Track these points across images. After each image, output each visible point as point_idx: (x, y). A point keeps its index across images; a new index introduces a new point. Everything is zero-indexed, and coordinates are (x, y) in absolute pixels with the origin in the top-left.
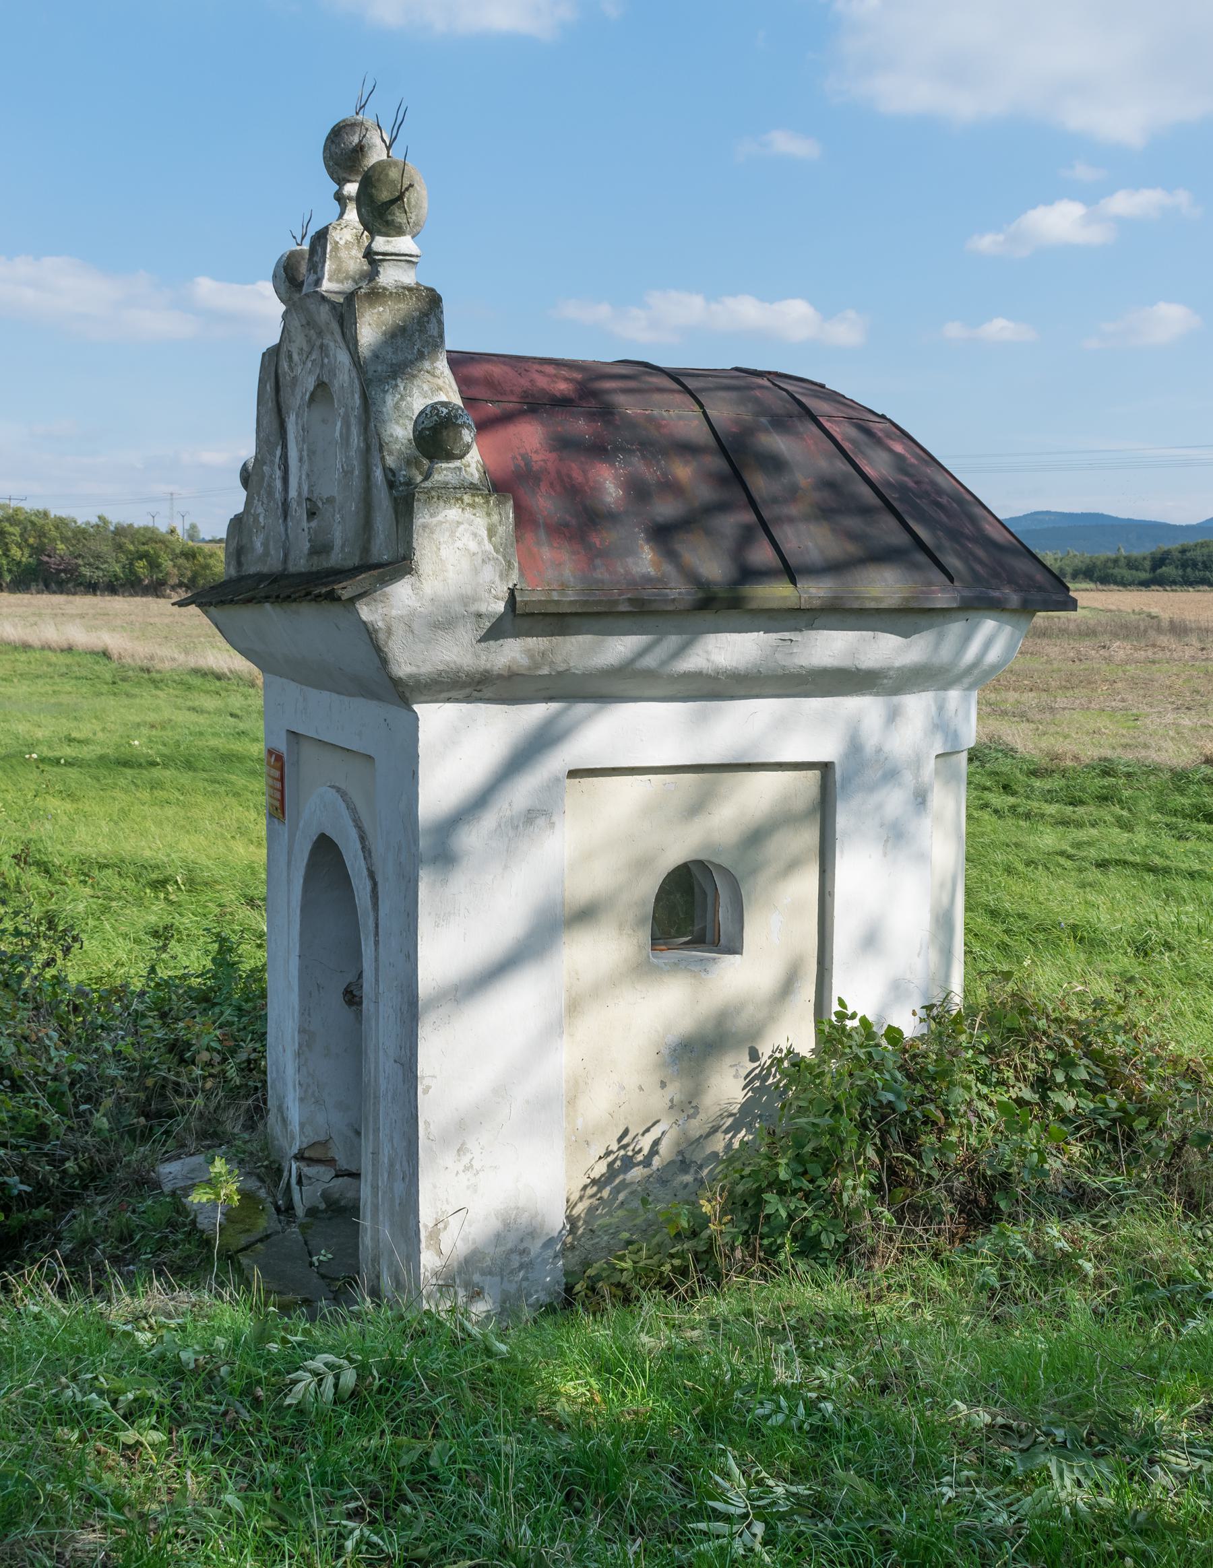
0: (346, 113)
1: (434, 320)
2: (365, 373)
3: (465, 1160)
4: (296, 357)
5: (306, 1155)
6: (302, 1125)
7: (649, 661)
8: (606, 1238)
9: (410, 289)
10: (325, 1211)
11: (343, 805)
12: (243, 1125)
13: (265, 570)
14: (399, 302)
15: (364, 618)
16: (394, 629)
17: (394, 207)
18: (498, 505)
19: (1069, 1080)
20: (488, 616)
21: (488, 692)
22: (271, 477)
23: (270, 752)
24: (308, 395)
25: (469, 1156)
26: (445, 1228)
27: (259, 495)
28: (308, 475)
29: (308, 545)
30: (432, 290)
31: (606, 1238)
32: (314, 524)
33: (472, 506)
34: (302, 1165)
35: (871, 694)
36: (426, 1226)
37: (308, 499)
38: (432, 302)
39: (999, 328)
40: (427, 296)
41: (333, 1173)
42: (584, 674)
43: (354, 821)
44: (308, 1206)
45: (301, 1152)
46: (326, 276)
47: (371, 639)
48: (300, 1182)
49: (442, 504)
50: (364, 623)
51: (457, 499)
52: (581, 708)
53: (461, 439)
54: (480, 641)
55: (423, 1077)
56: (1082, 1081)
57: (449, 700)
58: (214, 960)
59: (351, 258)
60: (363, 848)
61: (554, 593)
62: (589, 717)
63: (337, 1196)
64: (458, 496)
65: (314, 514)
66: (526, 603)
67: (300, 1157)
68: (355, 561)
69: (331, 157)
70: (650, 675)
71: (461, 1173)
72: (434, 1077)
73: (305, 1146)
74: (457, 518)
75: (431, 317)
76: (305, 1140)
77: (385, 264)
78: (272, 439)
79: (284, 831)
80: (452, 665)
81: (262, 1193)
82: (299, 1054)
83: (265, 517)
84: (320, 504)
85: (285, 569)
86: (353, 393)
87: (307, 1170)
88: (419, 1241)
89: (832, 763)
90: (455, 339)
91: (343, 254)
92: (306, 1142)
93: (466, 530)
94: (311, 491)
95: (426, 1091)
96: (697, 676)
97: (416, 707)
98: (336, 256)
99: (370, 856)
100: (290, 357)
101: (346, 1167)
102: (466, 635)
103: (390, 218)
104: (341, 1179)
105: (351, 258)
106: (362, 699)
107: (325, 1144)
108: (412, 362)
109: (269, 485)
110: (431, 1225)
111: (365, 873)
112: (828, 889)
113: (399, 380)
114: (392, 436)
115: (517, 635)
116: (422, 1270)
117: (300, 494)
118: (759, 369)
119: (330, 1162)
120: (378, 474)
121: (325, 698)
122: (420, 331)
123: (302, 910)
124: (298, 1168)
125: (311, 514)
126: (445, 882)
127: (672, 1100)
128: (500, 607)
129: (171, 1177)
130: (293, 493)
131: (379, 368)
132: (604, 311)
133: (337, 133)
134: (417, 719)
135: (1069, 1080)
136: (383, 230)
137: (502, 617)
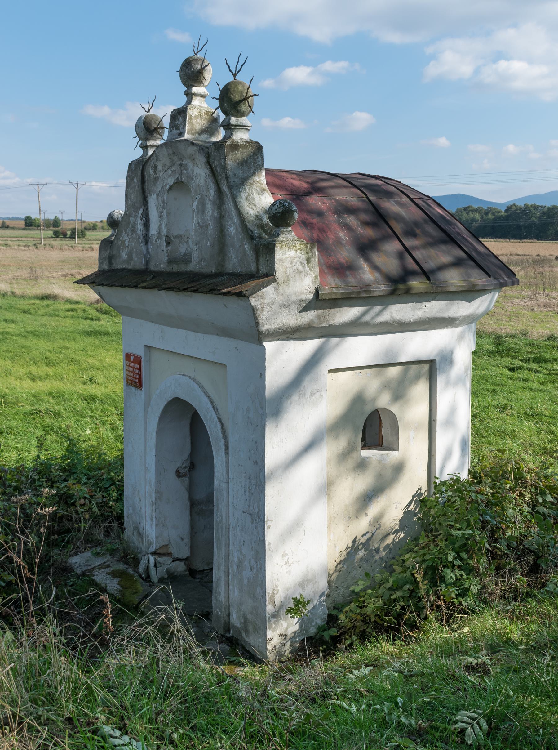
0: (190, 54)
1: (260, 157)
2: (230, 182)
3: (285, 559)
4: (159, 168)
5: (158, 552)
6: (157, 538)
7: (367, 318)
8: (343, 590)
9: (249, 143)
10: (167, 578)
11: (196, 385)
12: (104, 535)
13: (130, 267)
14: (245, 149)
15: (253, 304)
16: (264, 309)
17: (242, 104)
18: (311, 249)
19: (544, 501)
20: (305, 301)
21: (296, 336)
22: (135, 223)
23: (128, 356)
24: (168, 187)
25: (287, 557)
26: (277, 593)
27: (126, 231)
28: (167, 225)
29: (166, 258)
30: (258, 143)
31: (343, 590)
32: (169, 248)
33: (300, 249)
34: (156, 557)
35: (450, 328)
36: (269, 593)
37: (167, 236)
38: (258, 149)
39: (286, 122)
40: (257, 146)
41: (172, 560)
42: (339, 325)
43: (205, 393)
44: (159, 577)
45: (156, 550)
46: (186, 132)
47: (254, 314)
48: (155, 566)
49: (287, 249)
50: (252, 306)
51: (294, 246)
52: (334, 340)
53: (294, 217)
54: (299, 312)
55: (267, 521)
56: (550, 502)
57: (279, 340)
58: (67, 450)
59: (197, 123)
60: (213, 407)
61: (334, 289)
62: (337, 345)
63: (173, 570)
64: (294, 244)
65: (169, 243)
66: (323, 294)
67: (154, 553)
68: (213, 269)
69: (186, 74)
70: (367, 324)
71: (284, 566)
72: (272, 520)
73: (158, 547)
74: (294, 255)
75: (259, 155)
76: (159, 545)
77: (236, 130)
78: (137, 205)
79: (141, 395)
80: (286, 324)
81: (130, 571)
82: (153, 504)
83: (129, 242)
84: (172, 239)
85: (147, 269)
86: (208, 189)
87: (159, 559)
88: (266, 600)
89: (435, 360)
90: (267, 165)
91: (194, 121)
92: (159, 545)
93: (297, 261)
94: (168, 232)
95: (269, 528)
96: (386, 324)
97: (264, 344)
98: (191, 122)
99: (217, 410)
100: (156, 167)
101: (177, 556)
102: (294, 310)
103: (239, 109)
104: (175, 562)
105: (197, 123)
106: (216, 337)
107: (166, 546)
108: (250, 177)
109: (133, 227)
110: (271, 592)
111: (216, 419)
112: (433, 418)
113: (246, 186)
114: (248, 213)
115: (315, 309)
116: (267, 615)
117: (159, 233)
118: (370, 174)
119: (170, 554)
120: (232, 229)
121: (181, 332)
122: (254, 162)
123: (157, 433)
124: (155, 559)
125: (168, 243)
126: (277, 427)
127: (370, 522)
128: (311, 297)
129: (77, 565)
130: (153, 231)
131: (236, 180)
132: (106, 110)
133: (187, 64)
134: (265, 349)
135: (544, 501)
136: (235, 114)
137: (311, 301)
